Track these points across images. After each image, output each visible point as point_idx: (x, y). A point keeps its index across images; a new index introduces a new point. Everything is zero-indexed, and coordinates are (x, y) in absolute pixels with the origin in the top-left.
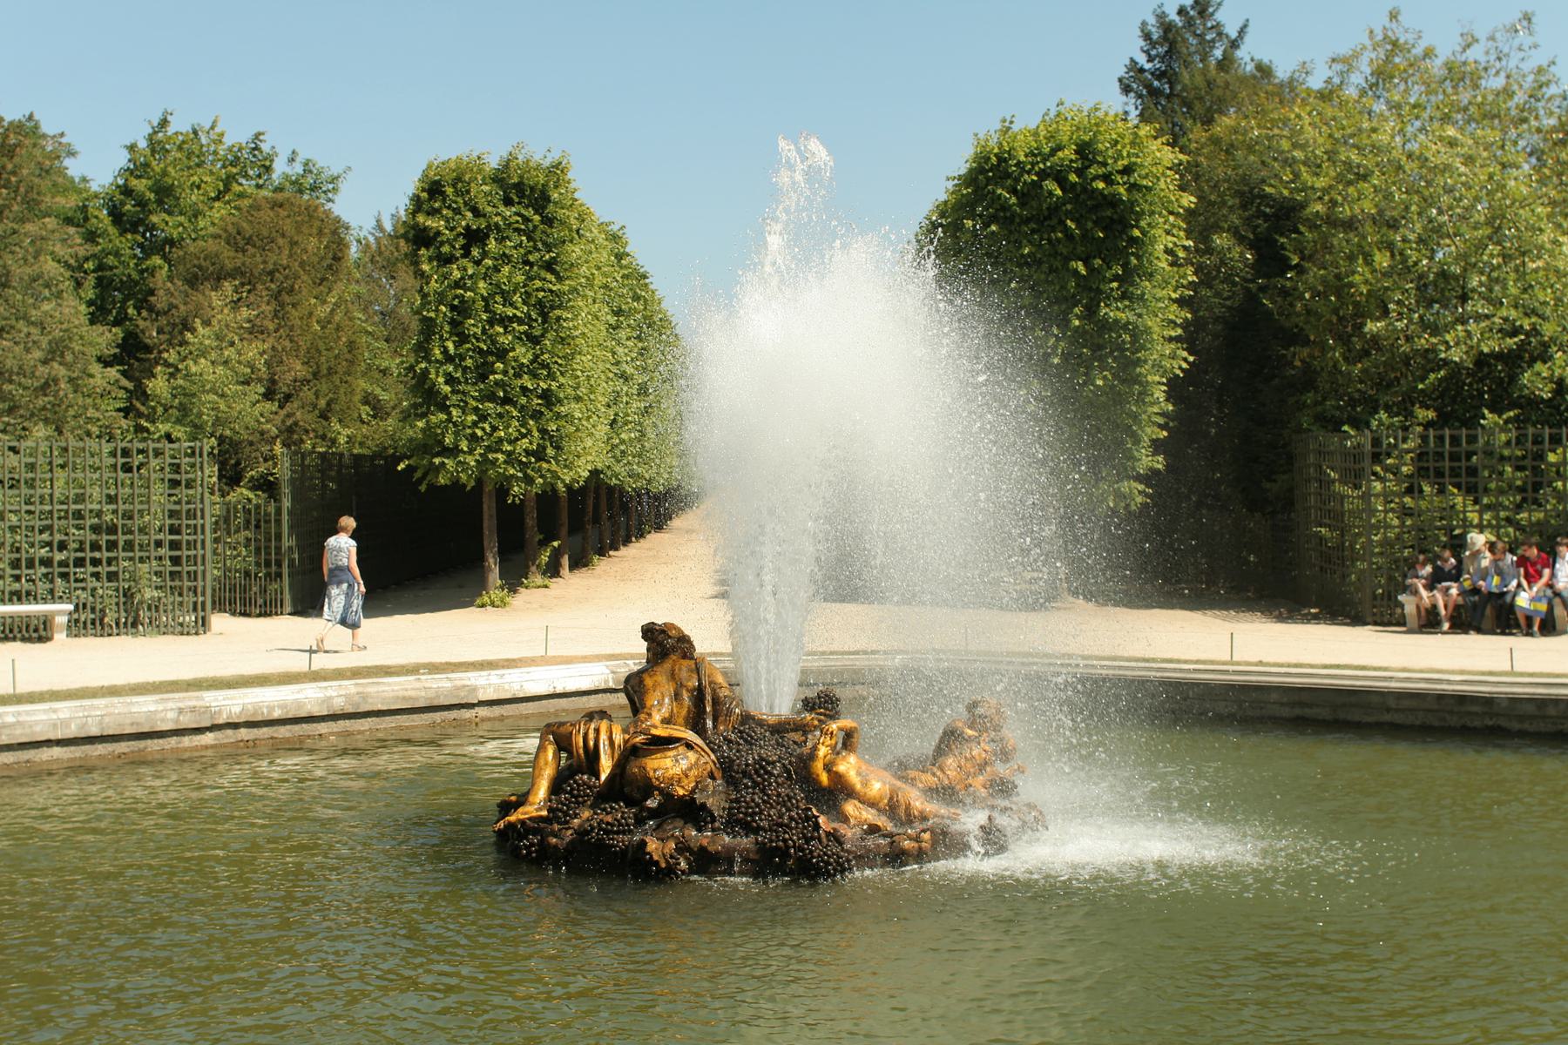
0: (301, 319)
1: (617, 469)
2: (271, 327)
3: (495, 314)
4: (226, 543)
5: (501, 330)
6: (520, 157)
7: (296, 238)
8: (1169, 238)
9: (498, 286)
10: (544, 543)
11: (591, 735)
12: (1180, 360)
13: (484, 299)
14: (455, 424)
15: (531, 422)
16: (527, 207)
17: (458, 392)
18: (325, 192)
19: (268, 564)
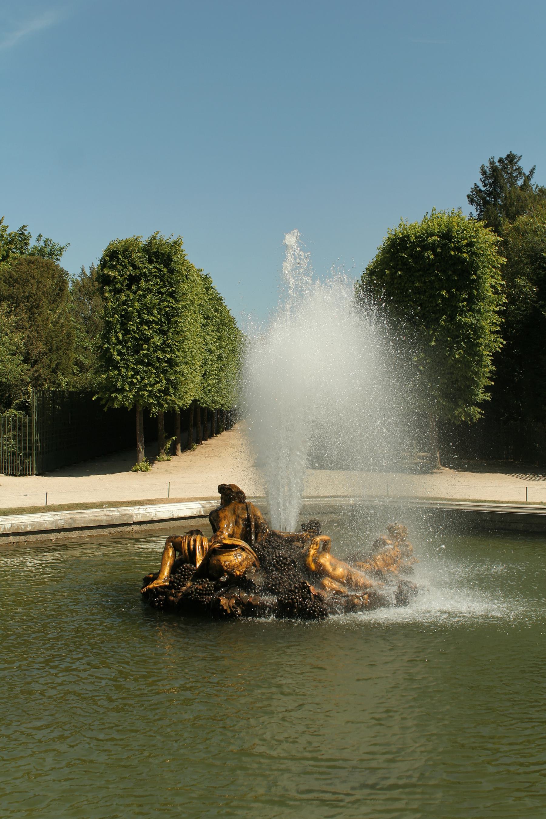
0: (43, 321)
1: (206, 399)
2: (27, 325)
3: (143, 319)
4: (3, 437)
5: (147, 328)
6: (157, 238)
7: (40, 280)
8: (493, 280)
9: (145, 305)
10: (168, 438)
11: (192, 543)
12: (500, 343)
13: (138, 311)
14: (122, 377)
15: (162, 375)
16: (160, 264)
17: (124, 360)
18: (56, 256)
19: (25, 449)
